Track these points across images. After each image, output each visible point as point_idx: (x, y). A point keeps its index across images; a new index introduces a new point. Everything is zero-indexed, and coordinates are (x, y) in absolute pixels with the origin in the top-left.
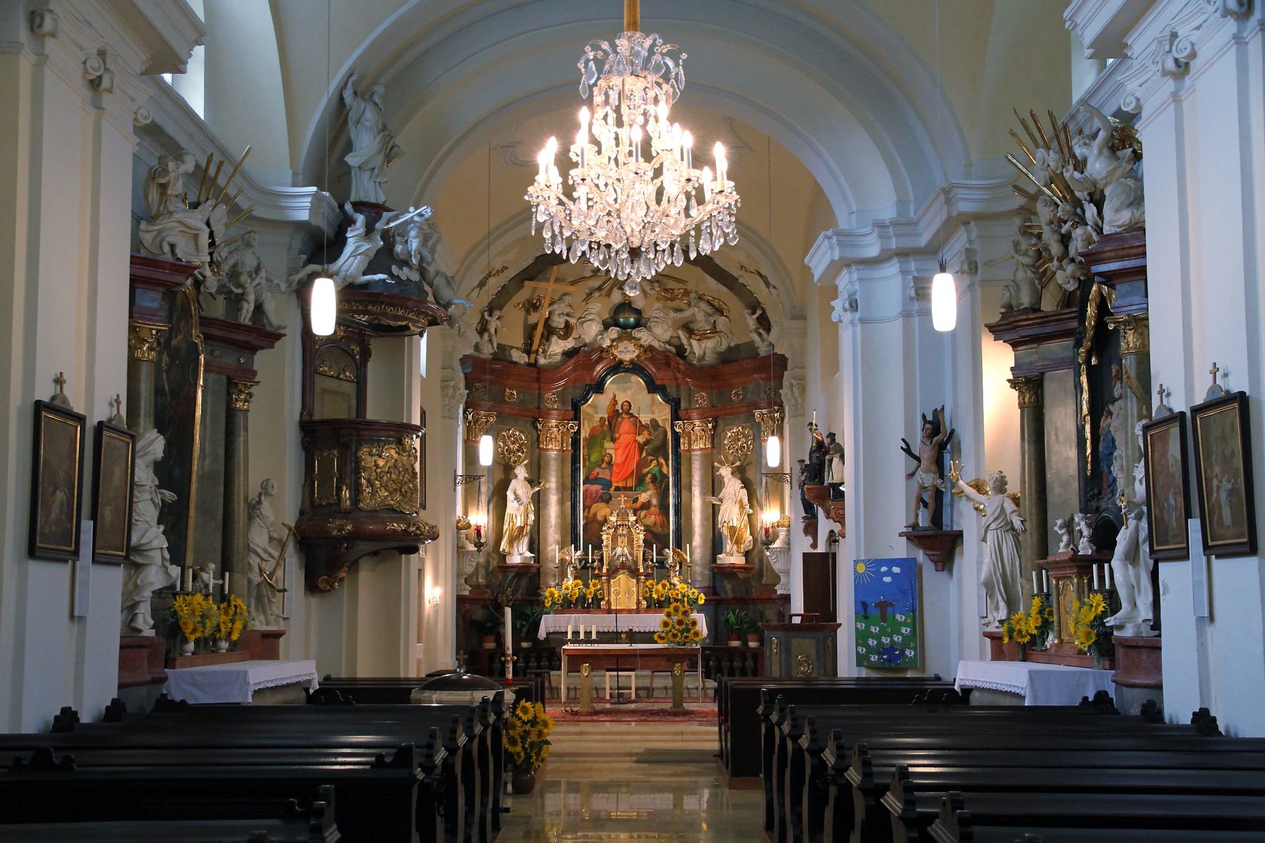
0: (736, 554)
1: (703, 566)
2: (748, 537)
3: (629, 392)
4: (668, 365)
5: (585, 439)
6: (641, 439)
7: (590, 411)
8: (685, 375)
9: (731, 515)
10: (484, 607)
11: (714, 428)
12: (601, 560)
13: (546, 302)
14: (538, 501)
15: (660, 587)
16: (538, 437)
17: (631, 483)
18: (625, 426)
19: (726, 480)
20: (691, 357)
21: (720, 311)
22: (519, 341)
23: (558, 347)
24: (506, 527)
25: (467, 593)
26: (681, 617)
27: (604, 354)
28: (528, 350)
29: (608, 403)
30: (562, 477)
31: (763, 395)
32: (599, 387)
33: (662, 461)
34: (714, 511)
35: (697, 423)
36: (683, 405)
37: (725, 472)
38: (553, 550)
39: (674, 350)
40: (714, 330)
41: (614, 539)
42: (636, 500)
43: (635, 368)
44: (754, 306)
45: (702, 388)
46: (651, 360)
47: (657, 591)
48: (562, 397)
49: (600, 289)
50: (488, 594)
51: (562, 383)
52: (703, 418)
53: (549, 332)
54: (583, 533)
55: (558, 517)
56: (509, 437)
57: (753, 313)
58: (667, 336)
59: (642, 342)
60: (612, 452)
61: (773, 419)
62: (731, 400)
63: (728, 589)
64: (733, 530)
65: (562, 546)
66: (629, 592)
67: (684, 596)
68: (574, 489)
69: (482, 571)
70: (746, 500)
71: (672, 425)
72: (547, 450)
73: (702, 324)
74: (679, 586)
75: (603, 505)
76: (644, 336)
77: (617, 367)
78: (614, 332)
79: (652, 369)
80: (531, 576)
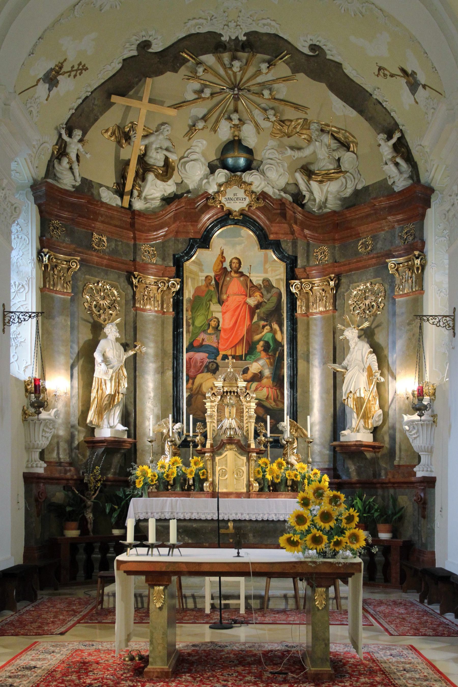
0: (362, 430)
1: (322, 445)
2: (377, 411)
3: (238, 248)
4: (283, 215)
5: (189, 300)
6: (252, 302)
7: (194, 268)
8: (303, 226)
9: (357, 383)
10: (66, 488)
11: (337, 286)
12: (205, 436)
13: (140, 132)
14: (133, 366)
15: (275, 466)
16: (134, 294)
17: (240, 351)
18: (234, 286)
19: (352, 344)
20: (310, 204)
21: (346, 146)
22: (110, 179)
23: (156, 190)
24: (93, 394)
25: (41, 471)
26: (326, 506)
27: (210, 203)
28: (120, 191)
29: (214, 260)
30: (163, 342)
31: (398, 241)
32: (205, 241)
33: (276, 326)
34: (336, 381)
35: (317, 281)
36: (300, 262)
37: (351, 334)
38: (151, 422)
39: (290, 199)
40: (339, 170)
41: (220, 410)
42: (246, 371)
43: (245, 220)
44: (390, 129)
45: (323, 242)
46: (262, 209)
47: (272, 472)
48: (162, 249)
49: (204, 118)
50: (71, 473)
51: (162, 232)
52: (324, 273)
53: (144, 167)
54: (182, 404)
55: (155, 389)
56: (99, 291)
57: (390, 137)
58: (282, 183)
59: (254, 188)
60: (219, 315)
61: (410, 268)
62: (357, 253)
63: (352, 471)
64: (360, 402)
65: (162, 416)
66: (238, 472)
67: (304, 478)
68: (177, 357)
69: (63, 445)
70: (375, 366)
71: (288, 285)
72: (144, 310)
73: (324, 163)
74: (297, 466)
75: (209, 375)
76: (255, 180)
77: (226, 218)
78: (221, 175)
79: (262, 219)
80: (124, 452)
